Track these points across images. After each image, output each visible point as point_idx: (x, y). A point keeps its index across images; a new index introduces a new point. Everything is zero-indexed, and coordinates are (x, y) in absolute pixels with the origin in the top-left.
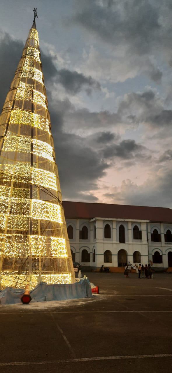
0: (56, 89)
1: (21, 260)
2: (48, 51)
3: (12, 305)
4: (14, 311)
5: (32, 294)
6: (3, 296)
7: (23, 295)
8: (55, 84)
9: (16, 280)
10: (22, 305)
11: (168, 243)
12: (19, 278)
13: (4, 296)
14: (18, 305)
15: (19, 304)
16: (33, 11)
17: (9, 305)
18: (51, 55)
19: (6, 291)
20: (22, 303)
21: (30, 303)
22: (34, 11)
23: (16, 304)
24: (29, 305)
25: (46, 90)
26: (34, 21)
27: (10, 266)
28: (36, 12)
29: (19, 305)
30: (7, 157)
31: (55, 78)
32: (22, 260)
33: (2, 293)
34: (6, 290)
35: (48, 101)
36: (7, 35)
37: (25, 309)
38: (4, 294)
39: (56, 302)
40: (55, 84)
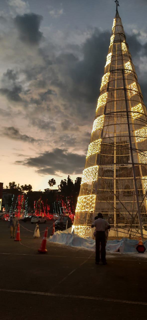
0: (142, 63)
1: (131, 216)
2: (131, 30)
3: (129, 253)
4: (132, 258)
5: (145, 244)
6: (121, 245)
7: (138, 245)
8: (141, 59)
9: (130, 232)
10: (138, 254)
11: (66, 247)
12: (131, 231)
13: (122, 246)
14: (134, 254)
15: (135, 252)
16: (115, 2)
17: (127, 253)
18: (135, 33)
19: (123, 241)
20: (138, 252)
21: (145, 253)
22: (115, 2)
23: (133, 253)
24: (145, 254)
25: (134, 66)
26: (116, 11)
27: (122, 221)
28: (117, 2)
29: (135, 253)
30: (108, 131)
31: (140, 53)
32: (132, 215)
33: (120, 243)
34: (123, 241)
35: (137, 101)
36: (97, 29)
37: (141, 257)
38: (122, 243)
39: (29, 148)
40: (141, 59)
